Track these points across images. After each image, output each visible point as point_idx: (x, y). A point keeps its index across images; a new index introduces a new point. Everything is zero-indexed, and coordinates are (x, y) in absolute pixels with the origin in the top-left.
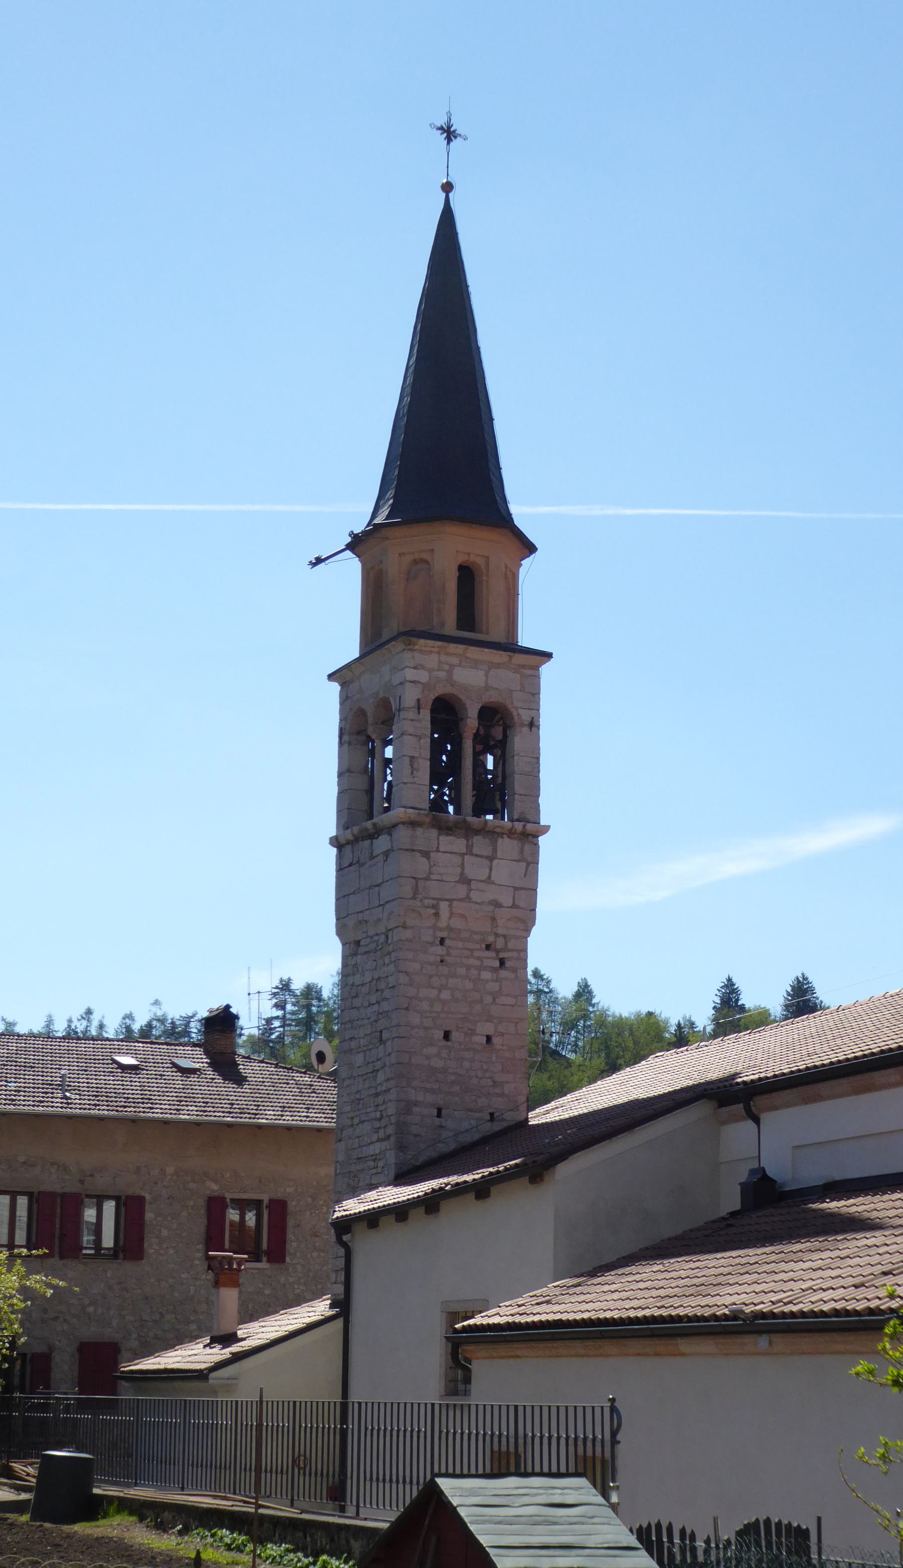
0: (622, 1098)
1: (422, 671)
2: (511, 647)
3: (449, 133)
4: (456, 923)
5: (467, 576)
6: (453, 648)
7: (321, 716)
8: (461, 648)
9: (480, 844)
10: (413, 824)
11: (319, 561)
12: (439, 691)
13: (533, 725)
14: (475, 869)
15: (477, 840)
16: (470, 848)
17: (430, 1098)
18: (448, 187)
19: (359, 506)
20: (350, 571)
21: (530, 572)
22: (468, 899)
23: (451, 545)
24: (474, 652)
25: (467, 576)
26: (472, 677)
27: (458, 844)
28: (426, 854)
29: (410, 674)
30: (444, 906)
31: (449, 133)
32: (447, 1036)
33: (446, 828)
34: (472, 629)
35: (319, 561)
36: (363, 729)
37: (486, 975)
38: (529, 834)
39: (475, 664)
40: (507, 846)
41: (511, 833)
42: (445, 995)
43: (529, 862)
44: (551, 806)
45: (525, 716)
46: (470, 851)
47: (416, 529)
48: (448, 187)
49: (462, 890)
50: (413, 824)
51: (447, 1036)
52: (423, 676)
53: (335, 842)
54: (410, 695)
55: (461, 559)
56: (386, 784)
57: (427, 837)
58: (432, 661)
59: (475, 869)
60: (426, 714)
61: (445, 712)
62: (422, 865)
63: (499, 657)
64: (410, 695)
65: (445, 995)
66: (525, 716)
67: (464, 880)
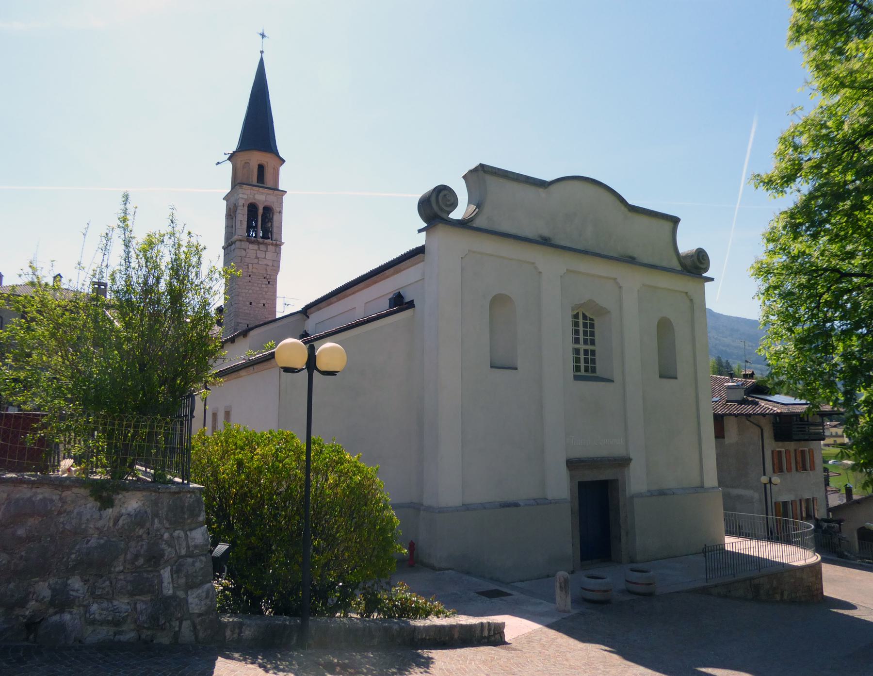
0: (754, 553)
1: (247, 195)
2: (275, 189)
3: (263, 35)
4: (254, 270)
5: (261, 168)
6: (254, 188)
7: (222, 208)
8: (257, 188)
9: (262, 247)
10: (241, 240)
11: (219, 163)
12: (250, 201)
13: (280, 212)
14: (261, 254)
15: (261, 246)
16: (259, 249)
17: (245, 322)
18: (262, 52)
19: (233, 145)
20: (229, 166)
21: (283, 170)
22: (258, 263)
23: (256, 158)
24: (261, 190)
25: (261, 168)
26: (261, 197)
27: (255, 247)
28: (245, 250)
29: (241, 196)
30: (250, 265)
31: (263, 35)
32: (251, 303)
33: (251, 242)
34: (263, 183)
35: (219, 163)
36: (231, 215)
37: (264, 286)
38: (278, 245)
39: (262, 193)
40: (270, 248)
41: (272, 244)
42: (250, 291)
43: (278, 253)
44: (285, 237)
45: (278, 210)
46: (259, 249)
47: (247, 153)
48: (262, 52)
49: (256, 261)
50: (241, 240)
51: (251, 303)
52: (245, 197)
53: (224, 248)
54: (241, 202)
55: (259, 162)
56: (797, 556)
57: (245, 244)
58: (248, 192)
59: (261, 254)
60: (246, 208)
61: (252, 208)
62: (243, 253)
63: (270, 192)
64: (241, 202)
65: (250, 291)
66: (278, 210)
67: (257, 258)
